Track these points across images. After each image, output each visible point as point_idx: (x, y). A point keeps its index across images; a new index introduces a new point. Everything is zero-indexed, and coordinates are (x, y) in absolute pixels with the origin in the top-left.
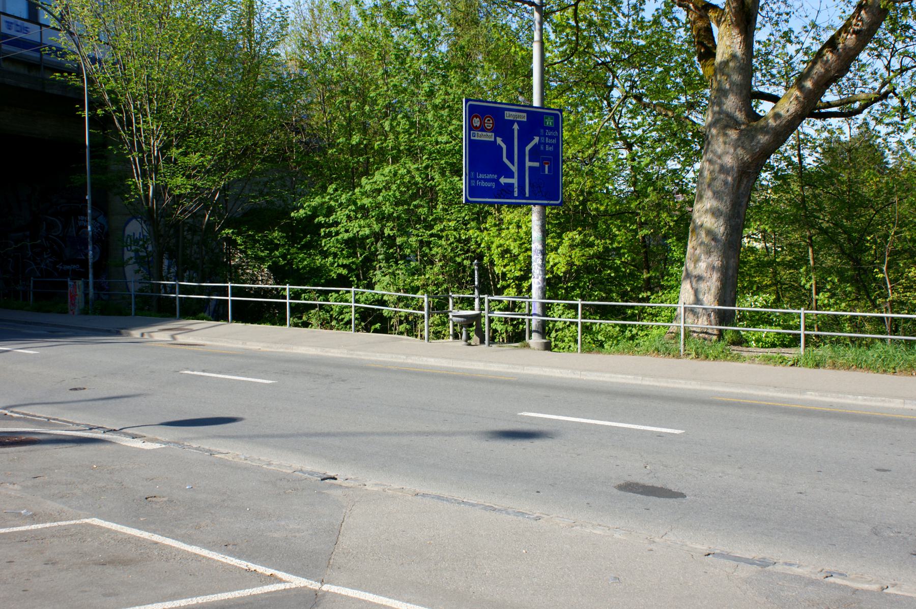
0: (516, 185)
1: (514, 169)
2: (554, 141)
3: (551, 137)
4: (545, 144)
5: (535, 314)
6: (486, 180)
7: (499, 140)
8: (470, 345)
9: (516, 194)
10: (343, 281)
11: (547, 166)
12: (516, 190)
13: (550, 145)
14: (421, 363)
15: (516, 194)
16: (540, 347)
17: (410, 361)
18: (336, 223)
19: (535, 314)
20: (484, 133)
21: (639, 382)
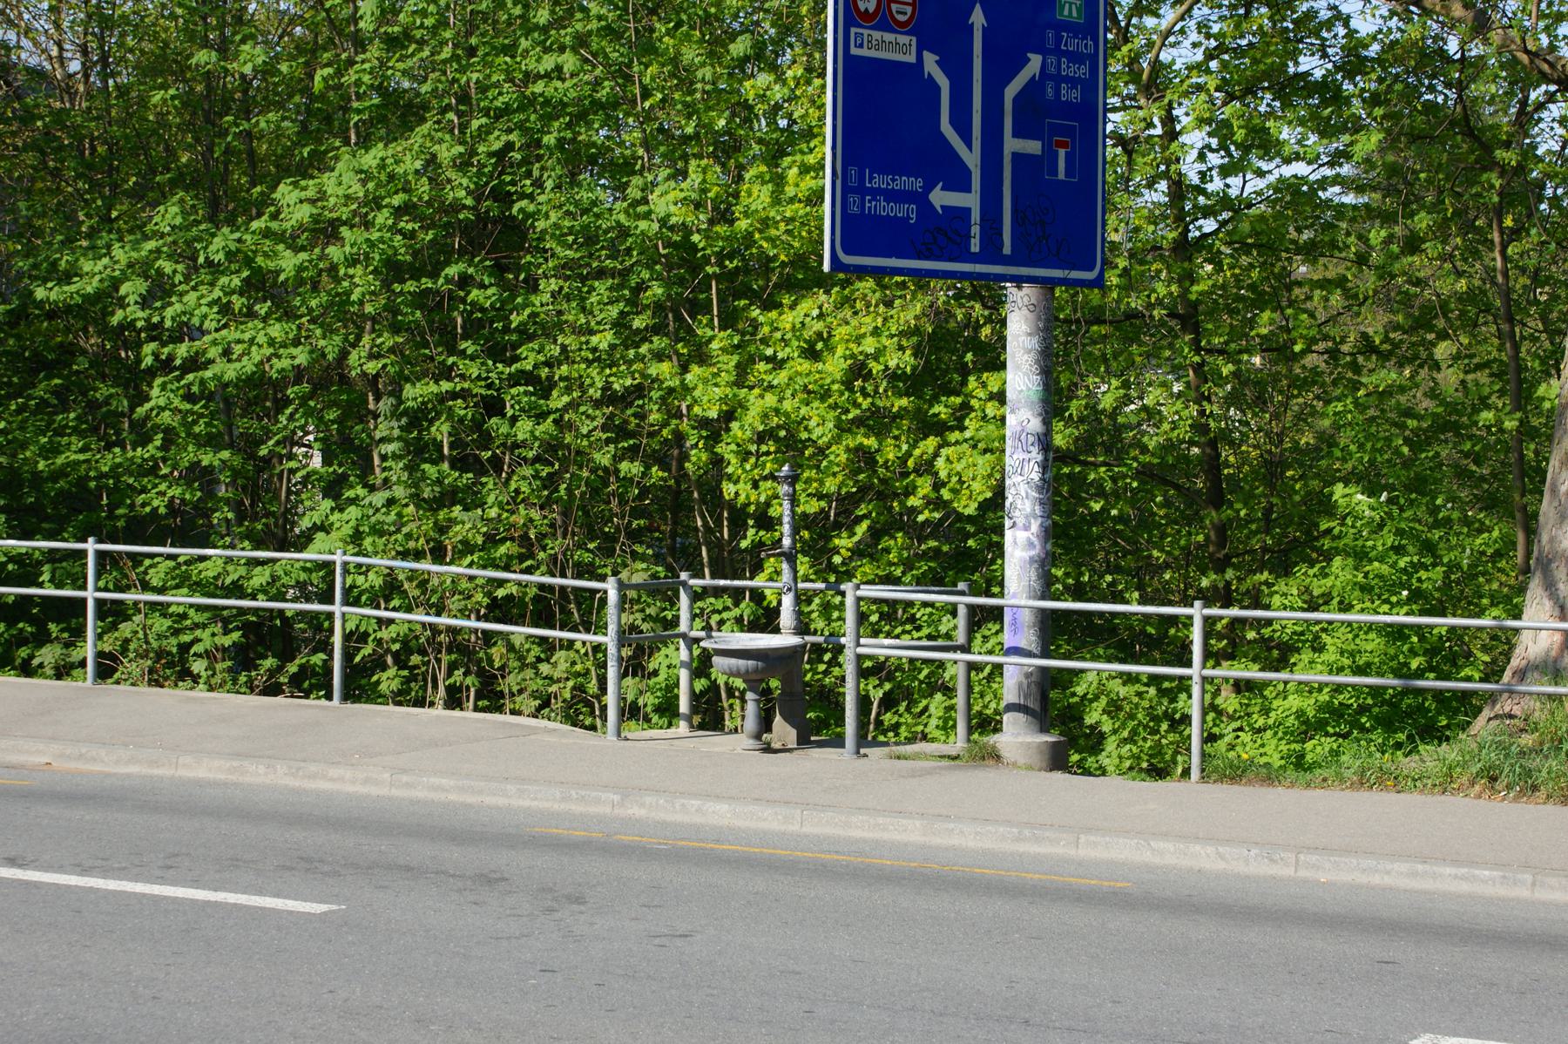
0: (976, 216)
1: (972, 159)
2: (1082, 71)
3: (1075, 58)
4: (1059, 79)
5: (1016, 651)
6: (893, 196)
7: (930, 62)
8: (768, 749)
9: (975, 247)
10: (187, 527)
11: (1062, 152)
12: (975, 230)
13: (1073, 82)
14: (679, 818)
15: (975, 247)
16: (1037, 760)
17: (635, 811)
18: (184, 330)
19: (1016, 651)
20: (889, 37)
21: (1524, 893)
